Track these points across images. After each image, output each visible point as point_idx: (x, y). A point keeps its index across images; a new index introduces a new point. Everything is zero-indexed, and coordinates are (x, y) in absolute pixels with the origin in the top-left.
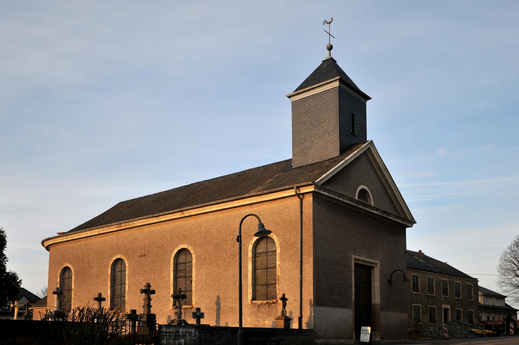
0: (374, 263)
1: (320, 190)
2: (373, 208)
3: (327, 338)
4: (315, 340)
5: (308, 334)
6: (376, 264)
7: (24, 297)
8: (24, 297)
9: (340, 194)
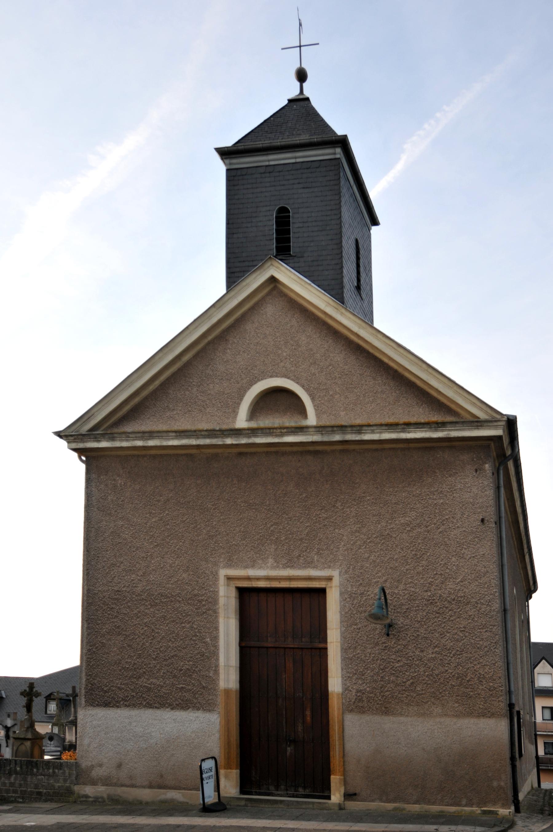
0: (294, 579)
1: (84, 442)
2: (279, 431)
3: (115, 785)
4: (76, 788)
5: (54, 772)
6: (329, 579)
7: (544, 661)
8: (544, 661)
9: (144, 432)
